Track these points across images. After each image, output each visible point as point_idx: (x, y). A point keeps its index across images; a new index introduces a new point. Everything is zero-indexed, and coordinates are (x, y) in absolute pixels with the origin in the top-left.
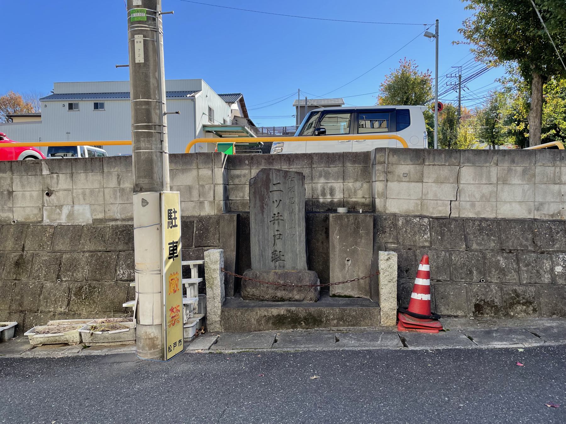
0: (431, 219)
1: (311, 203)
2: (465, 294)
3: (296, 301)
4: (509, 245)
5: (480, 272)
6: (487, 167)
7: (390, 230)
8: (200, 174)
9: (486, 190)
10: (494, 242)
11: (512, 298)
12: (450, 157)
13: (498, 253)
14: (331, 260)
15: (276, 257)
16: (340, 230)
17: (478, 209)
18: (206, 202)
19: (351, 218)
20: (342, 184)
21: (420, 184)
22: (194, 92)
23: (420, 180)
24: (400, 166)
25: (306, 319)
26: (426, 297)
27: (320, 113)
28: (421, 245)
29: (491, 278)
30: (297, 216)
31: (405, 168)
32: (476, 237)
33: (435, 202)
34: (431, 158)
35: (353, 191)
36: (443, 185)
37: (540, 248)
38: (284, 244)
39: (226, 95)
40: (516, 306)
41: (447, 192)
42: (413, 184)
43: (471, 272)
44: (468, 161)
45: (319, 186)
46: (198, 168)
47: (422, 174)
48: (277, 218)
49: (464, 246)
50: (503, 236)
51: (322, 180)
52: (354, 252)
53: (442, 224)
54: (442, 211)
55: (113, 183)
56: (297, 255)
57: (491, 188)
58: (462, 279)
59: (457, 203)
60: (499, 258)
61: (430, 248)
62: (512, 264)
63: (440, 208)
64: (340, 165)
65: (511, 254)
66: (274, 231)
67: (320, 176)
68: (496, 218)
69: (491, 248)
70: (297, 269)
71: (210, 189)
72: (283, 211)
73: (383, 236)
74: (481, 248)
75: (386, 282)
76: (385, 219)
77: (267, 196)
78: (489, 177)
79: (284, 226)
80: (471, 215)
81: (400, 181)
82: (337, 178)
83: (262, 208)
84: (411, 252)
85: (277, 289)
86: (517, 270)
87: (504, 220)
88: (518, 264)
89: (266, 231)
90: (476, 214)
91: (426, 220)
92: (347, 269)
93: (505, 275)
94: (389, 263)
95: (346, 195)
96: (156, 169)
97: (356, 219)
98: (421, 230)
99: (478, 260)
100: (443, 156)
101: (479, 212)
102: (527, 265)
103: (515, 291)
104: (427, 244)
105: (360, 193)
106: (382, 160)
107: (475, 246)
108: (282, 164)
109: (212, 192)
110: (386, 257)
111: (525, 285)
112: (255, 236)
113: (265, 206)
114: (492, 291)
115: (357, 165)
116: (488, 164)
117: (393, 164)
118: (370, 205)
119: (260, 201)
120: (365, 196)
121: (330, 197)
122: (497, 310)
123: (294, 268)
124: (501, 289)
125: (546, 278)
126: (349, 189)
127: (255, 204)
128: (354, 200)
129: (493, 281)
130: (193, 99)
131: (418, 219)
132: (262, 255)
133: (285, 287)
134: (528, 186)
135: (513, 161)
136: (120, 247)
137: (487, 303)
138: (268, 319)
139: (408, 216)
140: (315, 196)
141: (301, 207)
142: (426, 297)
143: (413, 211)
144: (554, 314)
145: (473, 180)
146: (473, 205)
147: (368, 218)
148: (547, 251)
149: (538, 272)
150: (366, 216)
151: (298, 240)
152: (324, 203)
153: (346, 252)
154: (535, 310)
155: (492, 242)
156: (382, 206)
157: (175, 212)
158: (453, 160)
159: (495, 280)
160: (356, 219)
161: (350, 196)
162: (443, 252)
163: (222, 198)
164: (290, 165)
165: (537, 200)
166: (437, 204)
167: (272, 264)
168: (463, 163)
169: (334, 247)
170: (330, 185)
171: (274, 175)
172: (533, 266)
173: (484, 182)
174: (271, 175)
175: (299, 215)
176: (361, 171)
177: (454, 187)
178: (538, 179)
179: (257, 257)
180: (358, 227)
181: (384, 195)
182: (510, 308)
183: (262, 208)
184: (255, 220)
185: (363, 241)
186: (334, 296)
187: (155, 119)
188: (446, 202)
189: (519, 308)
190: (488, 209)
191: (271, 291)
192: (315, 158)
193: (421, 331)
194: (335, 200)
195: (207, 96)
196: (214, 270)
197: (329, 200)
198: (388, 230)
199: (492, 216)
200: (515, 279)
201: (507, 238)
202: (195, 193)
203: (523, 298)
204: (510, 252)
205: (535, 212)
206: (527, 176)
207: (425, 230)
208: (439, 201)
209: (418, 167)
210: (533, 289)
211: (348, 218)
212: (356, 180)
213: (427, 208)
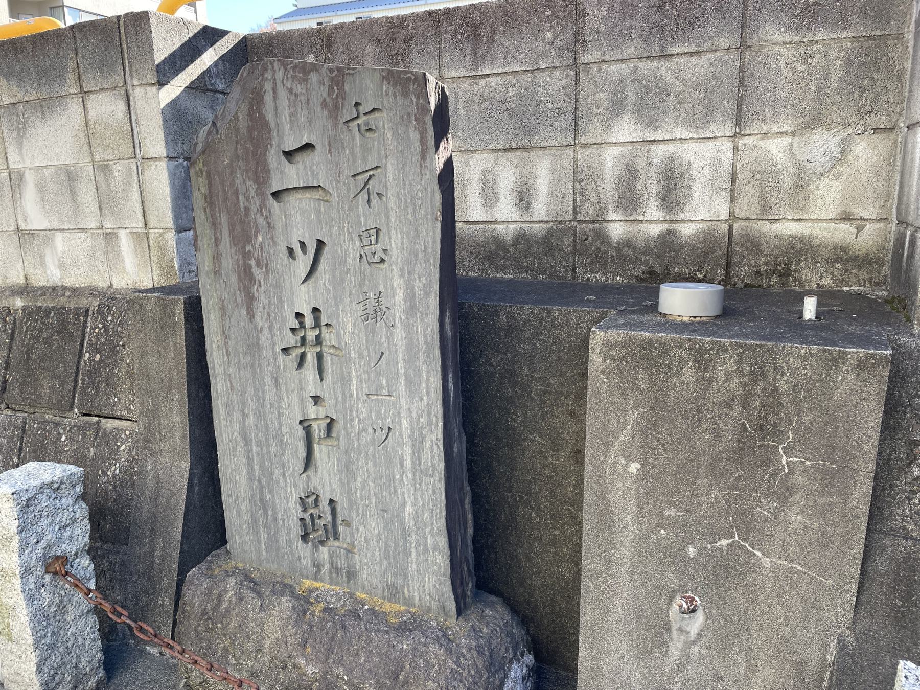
1: (567, 241)
8: (92, 115)
14: (588, 584)
15: (320, 523)
16: (648, 428)
18: (122, 234)
19: (725, 367)
20: (727, 145)
30: (399, 333)
35: (787, 182)
38: (348, 470)
45: (610, 161)
46: (84, 94)
48: (309, 338)
51: (626, 130)
52: (725, 573)
56: (405, 534)
64: (724, 42)
66: (302, 401)
67: (617, 108)
70: (408, 602)
71: (127, 181)
72: (338, 300)
77: (261, 220)
79: (345, 379)
82: (700, 118)
83: (246, 276)
89: (270, 395)
92: (675, 652)
95: (747, 206)
97: (758, 375)
105: (828, 196)
108: (446, 59)
109: (136, 195)
112: (229, 413)
113: (255, 271)
115: (822, 35)
118: (880, 262)
119: (235, 242)
120: (859, 211)
121: (658, 215)
123: (394, 592)
126: (765, 174)
127: (217, 258)
128: (788, 228)
132: (262, 505)
140: (589, 210)
141: (418, 284)
147: (846, 381)
150: (833, 363)
151: (408, 463)
152: (627, 243)
153: (673, 556)
160: (758, 375)
161: (765, 208)
163: (169, 221)
164: (477, 58)
167: (304, 551)
169: (607, 518)
171: (282, 94)
174: (268, 98)
175: (408, 328)
176: (848, 63)
179: (245, 506)
183: (246, 276)
184: (225, 336)
185: (796, 518)
194: (687, 230)
197: (655, 230)
202: (87, 196)
211: (701, 365)
212: (813, 122)
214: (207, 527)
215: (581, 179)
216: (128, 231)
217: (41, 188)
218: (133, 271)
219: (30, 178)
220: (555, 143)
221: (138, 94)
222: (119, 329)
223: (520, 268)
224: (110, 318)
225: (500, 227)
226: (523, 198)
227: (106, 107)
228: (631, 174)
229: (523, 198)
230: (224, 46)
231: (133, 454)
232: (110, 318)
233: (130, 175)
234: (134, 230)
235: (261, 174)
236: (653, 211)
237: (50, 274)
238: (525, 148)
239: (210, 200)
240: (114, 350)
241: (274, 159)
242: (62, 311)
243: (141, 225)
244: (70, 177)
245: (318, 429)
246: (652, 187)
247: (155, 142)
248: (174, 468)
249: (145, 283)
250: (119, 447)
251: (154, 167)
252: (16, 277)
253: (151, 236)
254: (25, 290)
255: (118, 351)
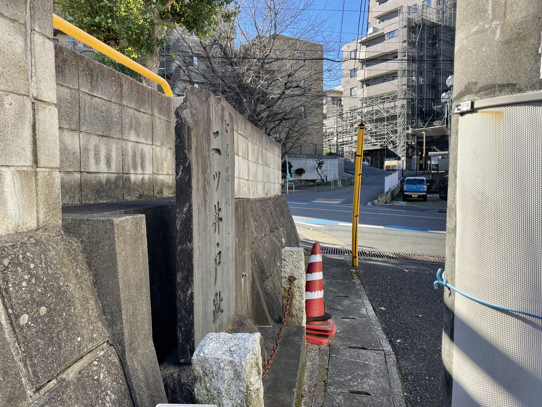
71: (20, 116)
109: (27, 133)
119: (202, 173)
216: (12, 169)
220: (116, 137)
222: (50, 272)
223: (109, 197)
224: (32, 266)
225: (101, 175)
231: (113, 372)
232: (32, 266)
233: (24, 111)
234: (19, 169)
238: (107, 137)
243: (29, 161)
249: (29, 225)
250: (97, 380)
251: (47, 110)
253: (40, 176)
255: (65, 292)
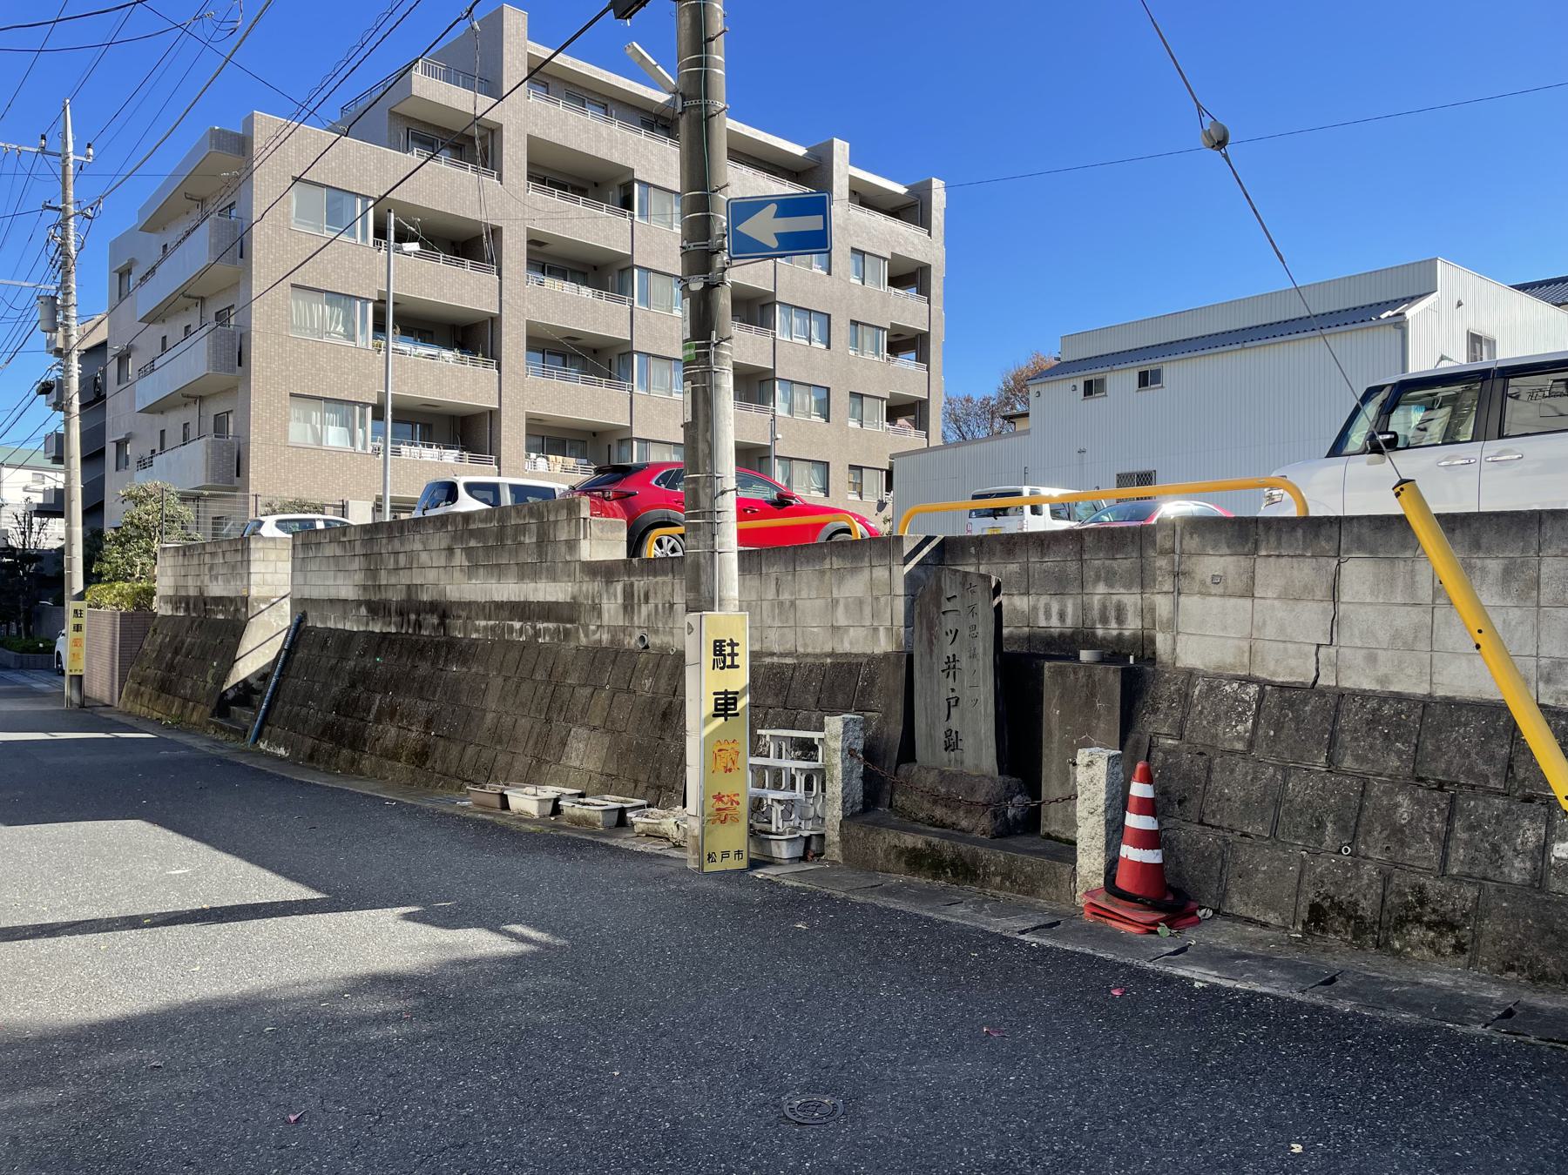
0: (1268, 688)
2: (1296, 875)
3: (962, 830)
4: (1437, 768)
5: (1343, 829)
6: (1405, 560)
7: (1170, 707)
9: (1406, 619)
10: (1400, 758)
11: (1407, 906)
12: (1317, 536)
13: (1403, 787)
16: (1062, 696)
17: (1382, 670)
21: (1248, 602)
22: (1404, 300)
23: (1248, 593)
24: (1206, 558)
25: (953, 864)
26: (1152, 857)
27: (1388, 390)
28: (1227, 746)
29: (1368, 847)
31: (1217, 563)
32: (1356, 739)
33: (1281, 646)
34: (1273, 539)
36: (1300, 606)
37: (1522, 784)
38: (962, 719)
39: (1548, 283)
40: (1409, 926)
41: (1310, 619)
42: (1233, 601)
43: (1321, 825)
44: (1360, 544)
47: (1253, 579)
48: (951, 666)
49: (1323, 759)
50: (1429, 746)
53: (1285, 699)
54: (1290, 667)
55: (770, 594)
57: (1416, 616)
58: (1297, 838)
59: (1332, 650)
60: (1400, 798)
61: (1244, 754)
62: (1431, 818)
63: (1293, 663)
65: (1436, 794)
67: (1098, 579)
68: (1430, 696)
69: (1389, 772)
73: (1152, 718)
74: (1365, 768)
75: (1085, 814)
76: (1167, 681)
78: (1412, 586)
80: (1367, 684)
81: (1204, 594)
82: (1128, 586)
83: (931, 643)
84: (1201, 762)
85: (935, 802)
86: (1442, 837)
87: (1449, 702)
88: (1449, 820)
90: (1380, 681)
91: (1253, 689)
93: (1402, 843)
94: (1091, 772)
96: (704, 578)
98: (1234, 710)
99: (1346, 798)
100: (1300, 533)
101: (1386, 676)
102: (1471, 828)
103: (1420, 890)
104: (1239, 746)
106: (1168, 545)
107: (1348, 763)
110: (1087, 760)
111: (1456, 879)
114: (1359, 877)
116: (1408, 554)
117: (1191, 555)
122: (1360, 928)
123: (977, 766)
124: (1387, 880)
125: (1518, 870)
129: (1371, 854)
130: (1400, 324)
131: (1235, 685)
132: (931, 736)
133: (948, 802)
134: (1518, 612)
135: (1476, 545)
136: (769, 702)
137: (1338, 907)
138: (901, 852)
139: (1220, 676)
140: (1088, 623)
142: (1152, 857)
143: (1233, 667)
144: (1511, 968)
145: (1372, 593)
146: (1372, 659)
147: (1111, 676)
148: (1541, 797)
149: (1495, 848)
152: (1104, 639)
154: (1459, 948)
155: (1393, 756)
156: (1169, 650)
157: (733, 644)
158: (1323, 543)
159: (1376, 854)
162: (1271, 770)
163: (902, 623)
164: (1043, 555)
165: (1544, 651)
166: (1286, 650)
168: (1347, 551)
169: (1050, 734)
170: (1115, 598)
172: (1485, 833)
173: (1399, 600)
177: (1324, 611)
178: (1547, 593)
180: (1093, 695)
181: (1172, 625)
182: (1395, 930)
183: (931, 643)
186: (1048, 836)
187: (704, 503)
188: (1307, 648)
189: (1417, 933)
190: (1409, 671)
191: (926, 805)
192: (1088, 540)
193: (1114, 923)
194: (1127, 633)
195: (1460, 304)
196: (835, 750)
197: (1115, 633)
198: (1163, 705)
199: (1421, 689)
200: (1430, 859)
201: (1439, 749)
202: (867, 610)
203: (1434, 911)
204: (1440, 787)
205: (1541, 686)
206: (1515, 585)
207: (1244, 712)
208: (1289, 645)
209: (1244, 562)
210: (1470, 892)
213: (1263, 660)
214: (907, 751)
215: (1085, 609)
217: (847, 607)
218: (884, 645)
219: (842, 602)
221: (895, 568)
226: (1062, 616)
227: (881, 573)
228: (1104, 608)
229: (1062, 616)
230: (934, 543)
235: (939, 607)
236: (1113, 625)
237: (845, 646)
239: (920, 614)
240: (873, 680)
241: (943, 599)
242: (849, 664)
244: (860, 602)
245: (953, 702)
246: (1112, 614)
247: (900, 589)
248: (896, 730)
252: (828, 649)
254: (832, 654)
